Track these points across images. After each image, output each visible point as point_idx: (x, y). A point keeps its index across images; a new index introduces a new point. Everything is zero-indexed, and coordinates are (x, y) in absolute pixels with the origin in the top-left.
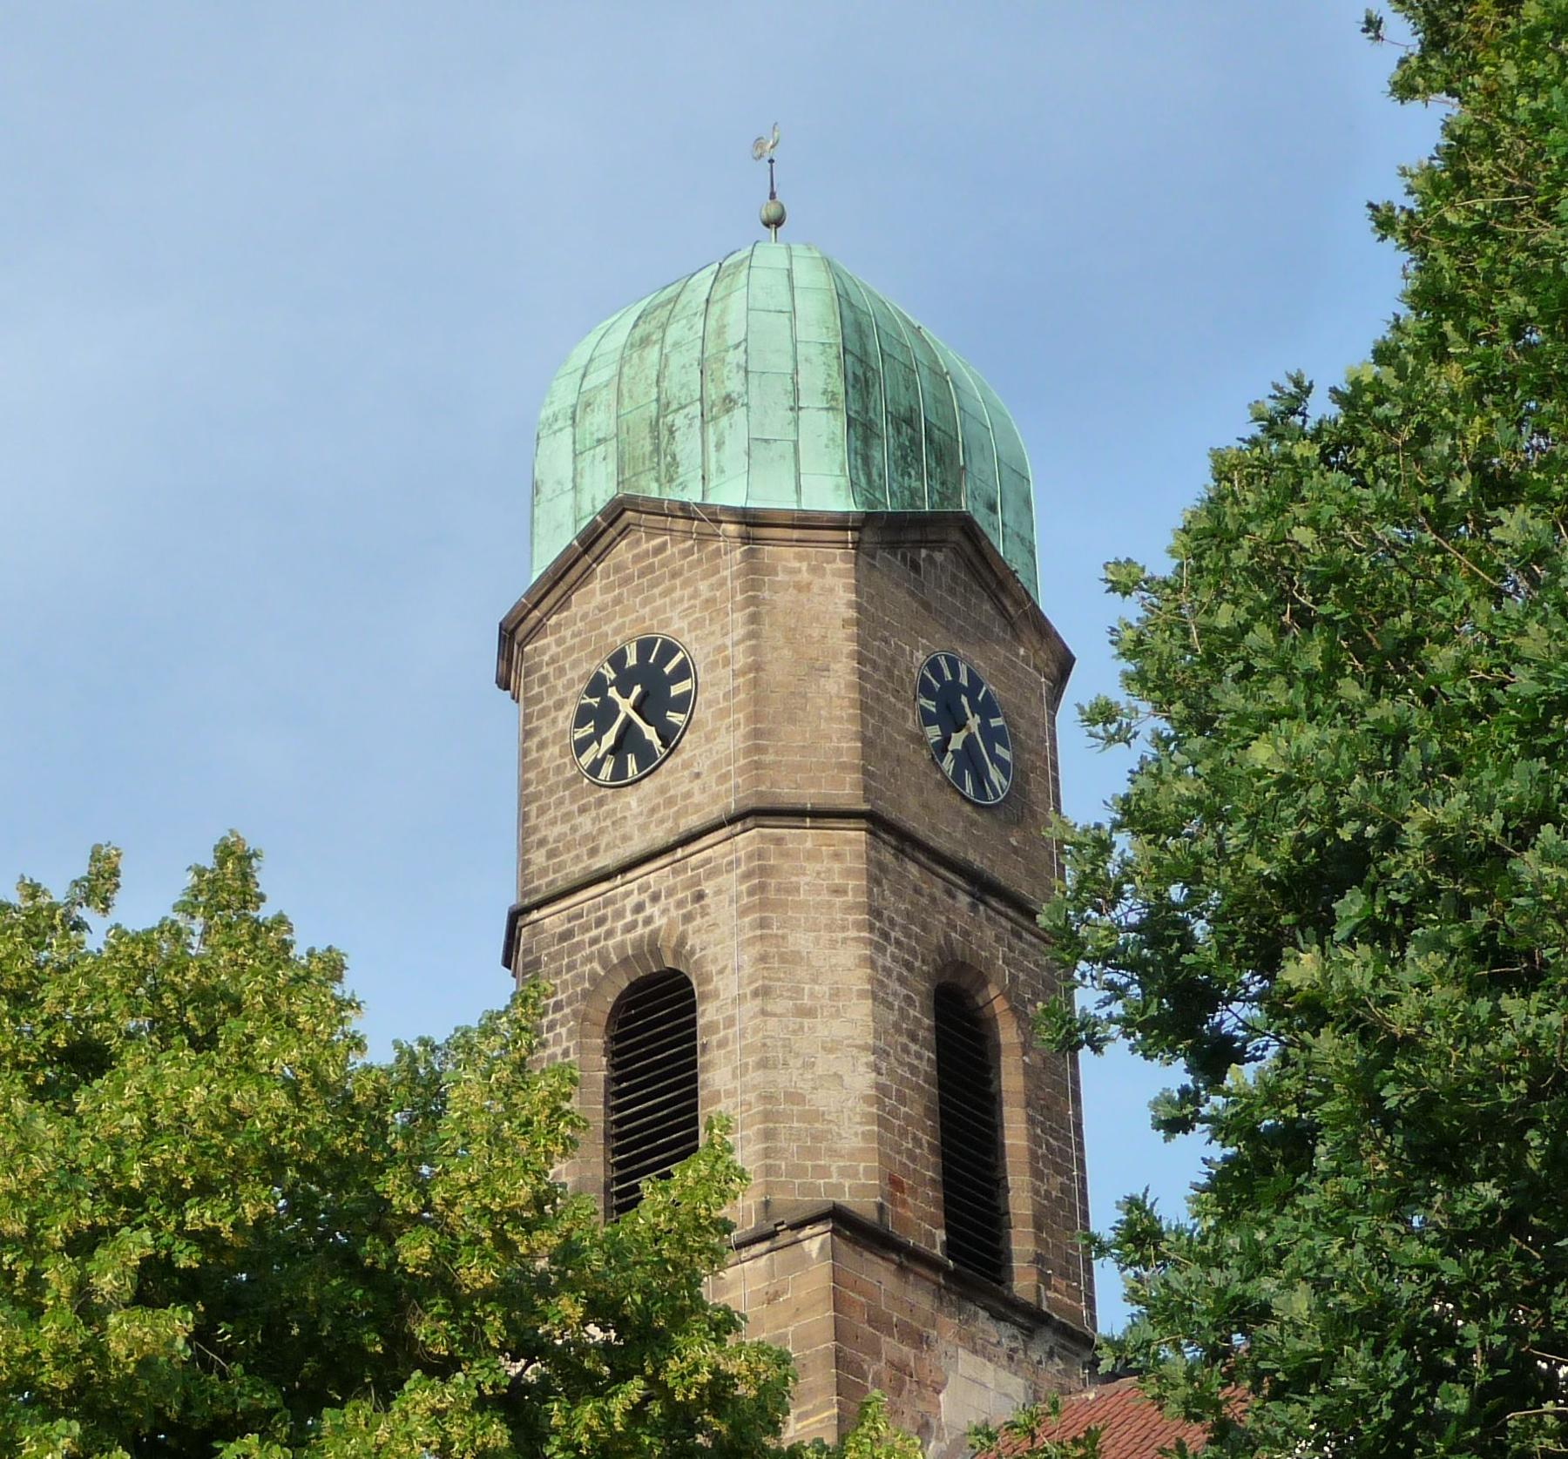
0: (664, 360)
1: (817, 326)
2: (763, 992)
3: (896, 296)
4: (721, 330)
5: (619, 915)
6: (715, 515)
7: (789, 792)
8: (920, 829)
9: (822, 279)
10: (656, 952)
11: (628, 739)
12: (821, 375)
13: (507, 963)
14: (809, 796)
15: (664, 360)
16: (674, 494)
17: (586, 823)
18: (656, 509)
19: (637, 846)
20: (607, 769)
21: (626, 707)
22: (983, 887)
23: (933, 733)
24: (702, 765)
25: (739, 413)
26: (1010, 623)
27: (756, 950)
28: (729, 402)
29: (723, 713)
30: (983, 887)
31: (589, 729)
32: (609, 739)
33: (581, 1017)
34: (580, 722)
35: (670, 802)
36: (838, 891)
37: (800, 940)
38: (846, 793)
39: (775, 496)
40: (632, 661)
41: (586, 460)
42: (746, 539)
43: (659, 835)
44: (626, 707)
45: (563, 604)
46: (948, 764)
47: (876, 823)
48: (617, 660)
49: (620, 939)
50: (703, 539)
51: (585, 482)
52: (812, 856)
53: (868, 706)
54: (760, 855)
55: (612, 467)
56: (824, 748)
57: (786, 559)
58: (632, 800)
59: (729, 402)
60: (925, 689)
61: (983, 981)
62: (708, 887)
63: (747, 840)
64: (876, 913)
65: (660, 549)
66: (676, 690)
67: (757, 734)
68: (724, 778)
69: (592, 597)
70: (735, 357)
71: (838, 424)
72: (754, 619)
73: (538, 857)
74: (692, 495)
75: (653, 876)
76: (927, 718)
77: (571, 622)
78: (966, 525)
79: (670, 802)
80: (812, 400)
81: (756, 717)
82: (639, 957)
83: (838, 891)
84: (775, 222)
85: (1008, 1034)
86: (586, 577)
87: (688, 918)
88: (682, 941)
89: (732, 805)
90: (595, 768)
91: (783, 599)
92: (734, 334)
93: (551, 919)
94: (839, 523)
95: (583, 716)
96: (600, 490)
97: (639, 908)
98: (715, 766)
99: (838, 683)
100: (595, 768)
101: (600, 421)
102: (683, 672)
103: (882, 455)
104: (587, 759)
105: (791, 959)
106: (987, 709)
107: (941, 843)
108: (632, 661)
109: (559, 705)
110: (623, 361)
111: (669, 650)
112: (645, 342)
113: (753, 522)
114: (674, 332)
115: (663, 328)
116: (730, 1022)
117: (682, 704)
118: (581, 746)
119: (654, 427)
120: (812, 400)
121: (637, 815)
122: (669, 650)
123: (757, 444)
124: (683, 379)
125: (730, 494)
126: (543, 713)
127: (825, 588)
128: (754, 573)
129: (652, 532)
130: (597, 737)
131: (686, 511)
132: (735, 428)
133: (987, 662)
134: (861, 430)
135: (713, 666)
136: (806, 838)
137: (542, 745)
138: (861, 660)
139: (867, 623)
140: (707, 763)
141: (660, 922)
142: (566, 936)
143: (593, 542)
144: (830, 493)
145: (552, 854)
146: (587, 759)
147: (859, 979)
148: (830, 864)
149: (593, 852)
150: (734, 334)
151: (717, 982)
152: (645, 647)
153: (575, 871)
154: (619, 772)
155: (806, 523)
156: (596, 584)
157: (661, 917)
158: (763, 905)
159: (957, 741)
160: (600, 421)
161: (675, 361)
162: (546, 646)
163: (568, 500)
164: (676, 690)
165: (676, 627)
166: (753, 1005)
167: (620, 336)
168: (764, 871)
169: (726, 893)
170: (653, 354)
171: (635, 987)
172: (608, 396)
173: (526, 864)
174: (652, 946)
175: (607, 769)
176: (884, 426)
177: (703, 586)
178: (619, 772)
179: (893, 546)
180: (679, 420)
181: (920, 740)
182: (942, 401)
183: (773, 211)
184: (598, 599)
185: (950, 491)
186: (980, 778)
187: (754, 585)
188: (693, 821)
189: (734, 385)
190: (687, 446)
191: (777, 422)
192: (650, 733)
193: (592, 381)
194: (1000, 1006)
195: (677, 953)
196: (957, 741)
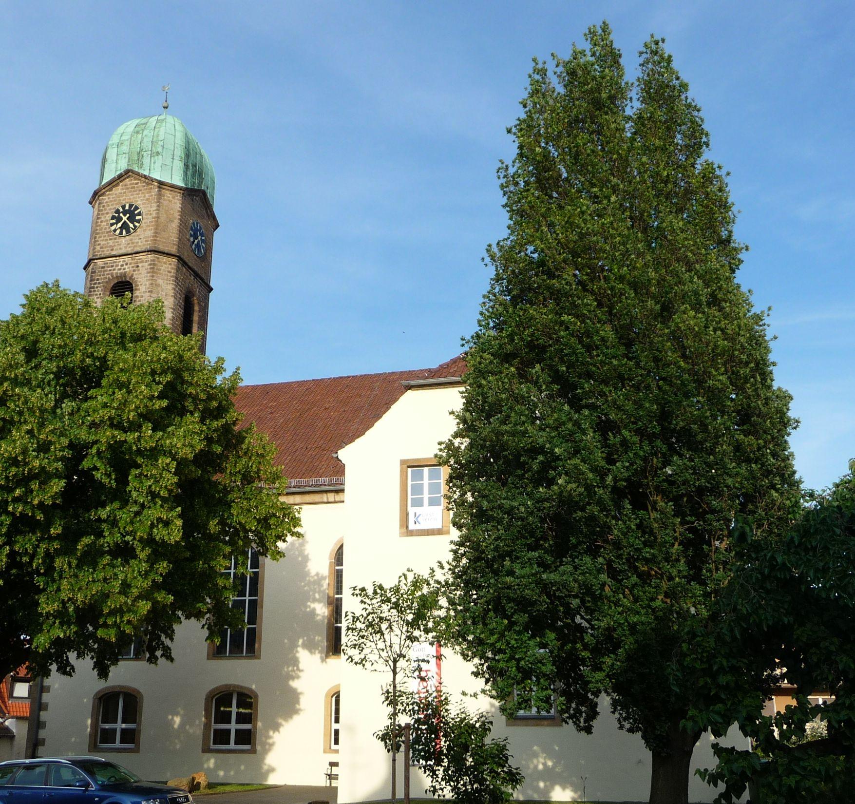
0: (143, 138)
1: (180, 141)
2: (151, 292)
3: (193, 137)
4: (158, 136)
5: (117, 266)
6: (152, 180)
7: (161, 248)
8: (186, 260)
9: (181, 129)
10: (125, 277)
11: (125, 226)
12: (179, 153)
13: (85, 269)
14: (166, 250)
15: (143, 138)
16: (141, 171)
17: (111, 243)
18: (138, 174)
19: (123, 251)
20: (118, 232)
21: (125, 218)
22: (197, 275)
23: (192, 239)
24: (142, 237)
25: (160, 157)
26: (208, 216)
27: (150, 282)
28: (158, 153)
29: (148, 226)
30: (197, 275)
31: (114, 221)
32: (120, 225)
33: (105, 287)
34: (112, 219)
35: (133, 243)
36: (170, 272)
37: (160, 282)
38: (174, 250)
39: (166, 179)
40: (127, 208)
41: (119, 157)
42: (159, 187)
43: (129, 250)
44: (125, 218)
45: (111, 190)
46: (193, 247)
47: (180, 258)
48: (123, 207)
49: (117, 271)
50: (148, 184)
51: (119, 162)
52: (165, 263)
53: (180, 231)
54: (154, 260)
55: (127, 160)
56: (170, 239)
57: (167, 194)
58: (123, 240)
59: (158, 153)
60: (192, 229)
61: (194, 296)
62: (140, 265)
63: (151, 256)
64: (177, 278)
65: (137, 183)
66: (137, 218)
67: (156, 233)
68: (147, 241)
69: (118, 190)
70: (161, 143)
71: (182, 165)
72: (158, 206)
73: (98, 248)
74: (146, 173)
75: (127, 259)
76: (191, 236)
77: (112, 194)
78: (204, 193)
79: (133, 243)
80: (177, 158)
81: (156, 229)
82: (121, 276)
83: (170, 272)
84: (166, 108)
85: (196, 308)
86: (117, 185)
87: (134, 271)
88: (132, 275)
89: (148, 247)
90: (115, 231)
91: (166, 203)
92: (161, 138)
93: (100, 263)
94: (180, 188)
95: (113, 218)
96: (123, 166)
97: (122, 265)
98: (145, 238)
99: (175, 225)
100: (115, 231)
101: (125, 148)
102: (139, 214)
103: (190, 173)
104: (113, 228)
105: (158, 285)
106: (202, 235)
107: (190, 264)
108: (127, 208)
109: (107, 213)
110: (132, 136)
111: (137, 208)
112: (138, 132)
113: (161, 184)
114: (145, 132)
115: (143, 130)
116: (142, 296)
117: (139, 221)
118: (112, 225)
119: (138, 154)
120: (177, 158)
121: (124, 244)
122: (137, 208)
123: (164, 165)
124: (147, 144)
125: (156, 175)
126: (103, 214)
127: (175, 203)
128: (160, 195)
129: (135, 179)
130: (117, 223)
131: (145, 177)
132: (159, 160)
133: (202, 223)
134: (186, 166)
135: (147, 214)
136: (164, 259)
137: (102, 222)
138: (181, 220)
139: (183, 212)
140: (143, 237)
141: (127, 270)
142: (103, 267)
143: (120, 177)
144: (178, 181)
145: (101, 248)
146: (113, 228)
147: (172, 293)
148: (168, 266)
149: (112, 250)
150: (161, 138)
151: (140, 287)
152: (131, 206)
153: (107, 253)
154: (121, 233)
155: (173, 186)
156: (120, 187)
157: (128, 269)
158: (153, 272)
159: (196, 242)
160: (125, 148)
161: (145, 140)
162: (105, 198)
163: (114, 165)
164: (137, 218)
165: (139, 203)
166: (148, 294)
167: (131, 129)
168: (154, 264)
169: (144, 267)
170: (140, 136)
171: (118, 283)
172: (127, 143)
173: (94, 249)
174: (125, 275)
175: (118, 232)
176: (191, 167)
177: (147, 195)
178: (121, 233)
179: (189, 195)
180: (145, 154)
181: (189, 240)
182: (202, 162)
183: (165, 105)
184: (120, 191)
185: (200, 184)
186: (199, 250)
187: (160, 198)
188: (138, 249)
189: (160, 150)
190: (146, 160)
191: (168, 161)
192: (131, 225)
193: (123, 138)
194: (196, 302)
195: (130, 278)
196: (196, 242)
